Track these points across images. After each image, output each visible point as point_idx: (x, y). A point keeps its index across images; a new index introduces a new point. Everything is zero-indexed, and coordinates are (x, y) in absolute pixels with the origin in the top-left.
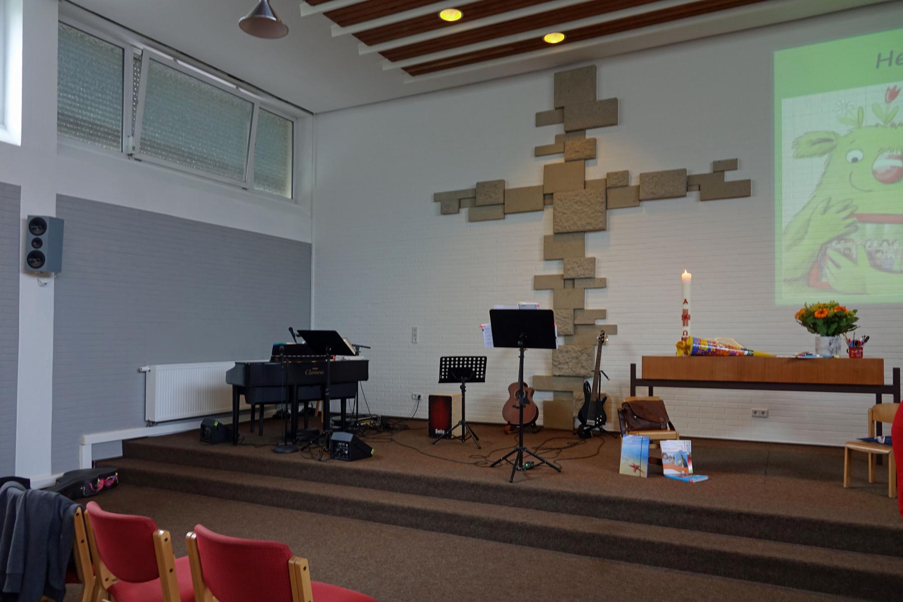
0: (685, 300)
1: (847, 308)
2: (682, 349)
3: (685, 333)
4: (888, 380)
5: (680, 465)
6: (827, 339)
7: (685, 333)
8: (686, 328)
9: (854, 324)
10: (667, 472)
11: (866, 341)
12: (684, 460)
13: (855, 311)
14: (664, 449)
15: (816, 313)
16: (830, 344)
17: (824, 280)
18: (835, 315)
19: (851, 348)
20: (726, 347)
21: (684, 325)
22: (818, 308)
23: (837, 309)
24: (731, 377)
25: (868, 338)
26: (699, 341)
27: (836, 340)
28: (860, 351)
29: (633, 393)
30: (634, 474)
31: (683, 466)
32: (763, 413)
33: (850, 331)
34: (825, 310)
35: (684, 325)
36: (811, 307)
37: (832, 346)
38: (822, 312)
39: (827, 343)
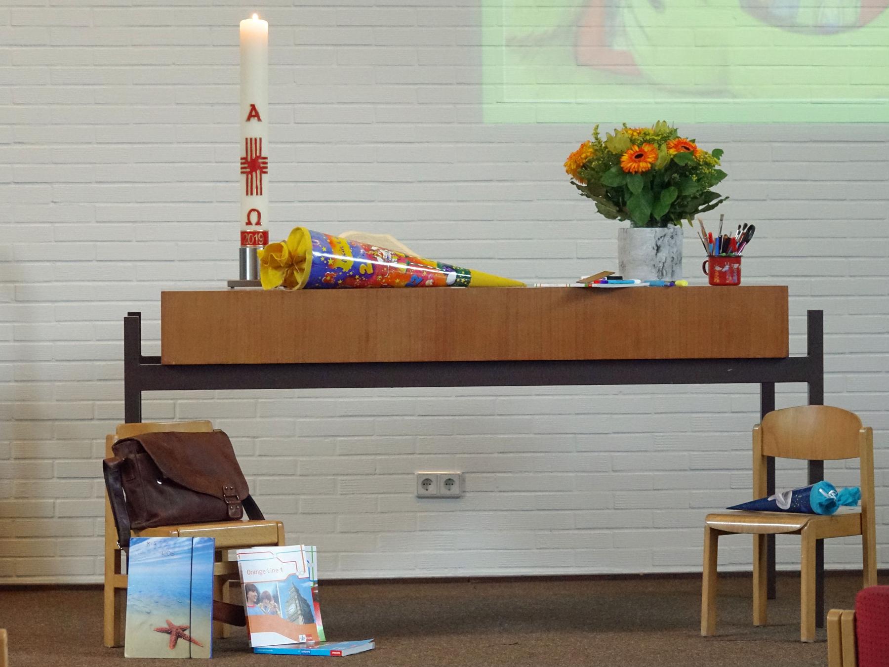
0: (253, 107)
1: (700, 146)
2: (277, 267)
3: (254, 218)
4: (798, 347)
5: (293, 619)
6: (650, 234)
7: (254, 218)
8: (256, 202)
9: (713, 189)
10: (258, 640)
11: (746, 238)
12: (303, 601)
13: (718, 153)
14: (250, 572)
15: (625, 158)
16: (658, 249)
17: (619, 45)
18: (672, 165)
19: (713, 260)
20: (400, 260)
21: (249, 191)
22: (629, 144)
23: (676, 146)
24: (418, 351)
25: (752, 228)
26: (330, 245)
27: (672, 237)
28: (736, 266)
29: (133, 412)
30: (172, 654)
31: (301, 621)
32: (449, 482)
33: (704, 210)
34: (646, 148)
35: (249, 191)
36: (610, 139)
37: (663, 255)
38: (639, 156)
39: (648, 248)
